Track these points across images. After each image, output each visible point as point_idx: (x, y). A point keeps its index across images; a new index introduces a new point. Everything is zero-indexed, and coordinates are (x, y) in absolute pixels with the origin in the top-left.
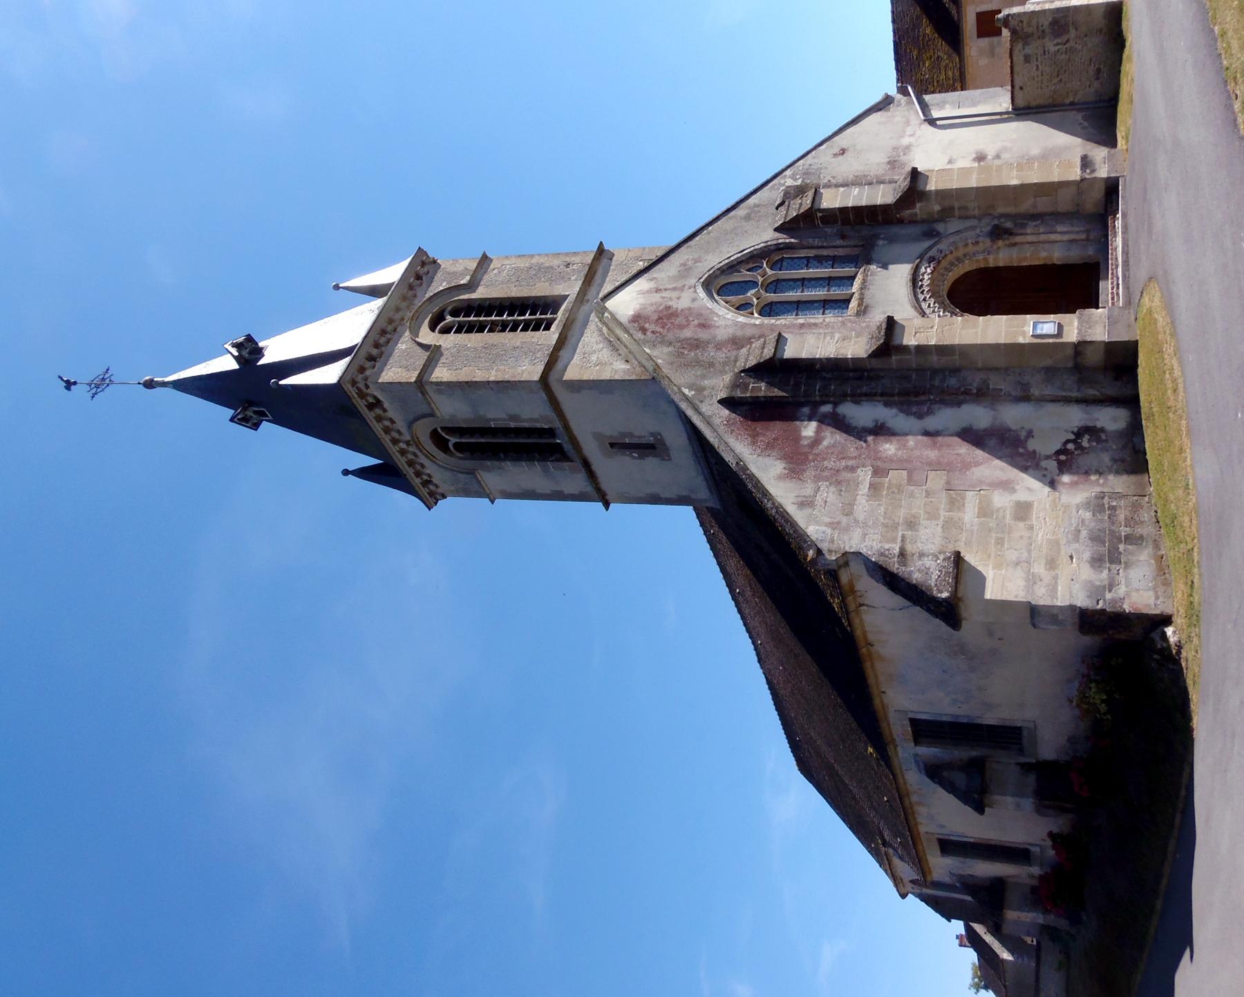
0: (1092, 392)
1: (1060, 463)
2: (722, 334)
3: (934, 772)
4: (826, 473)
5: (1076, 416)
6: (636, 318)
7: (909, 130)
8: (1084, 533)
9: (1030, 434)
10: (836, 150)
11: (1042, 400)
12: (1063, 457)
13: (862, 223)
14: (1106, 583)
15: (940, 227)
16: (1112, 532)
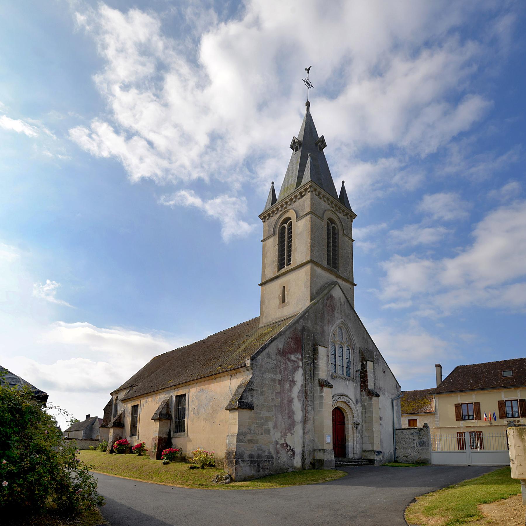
0: (306, 454)
1: (283, 444)
2: (326, 328)
3: (167, 404)
4: (279, 363)
5: (298, 450)
6: (332, 297)
7: (390, 395)
8: (261, 452)
9: (292, 434)
10: (384, 370)
11: (304, 438)
12: (285, 445)
13: (361, 378)
14: (245, 459)
15: (359, 405)
16: (261, 461)
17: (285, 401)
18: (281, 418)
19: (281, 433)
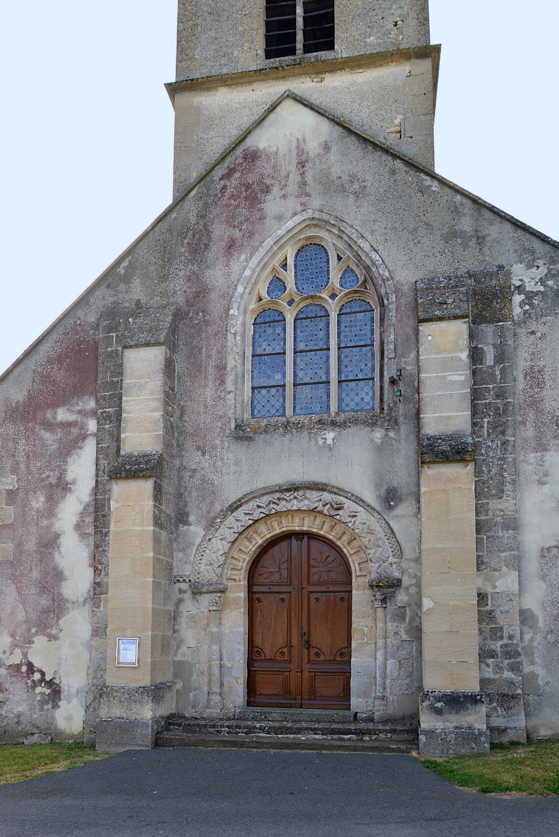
1: (19, 666)
2: (215, 276)
4: (10, 444)
9: (52, 638)
12: (24, 669)
17: (31, 545)
18: (15, 594)
19: (13, 635)
